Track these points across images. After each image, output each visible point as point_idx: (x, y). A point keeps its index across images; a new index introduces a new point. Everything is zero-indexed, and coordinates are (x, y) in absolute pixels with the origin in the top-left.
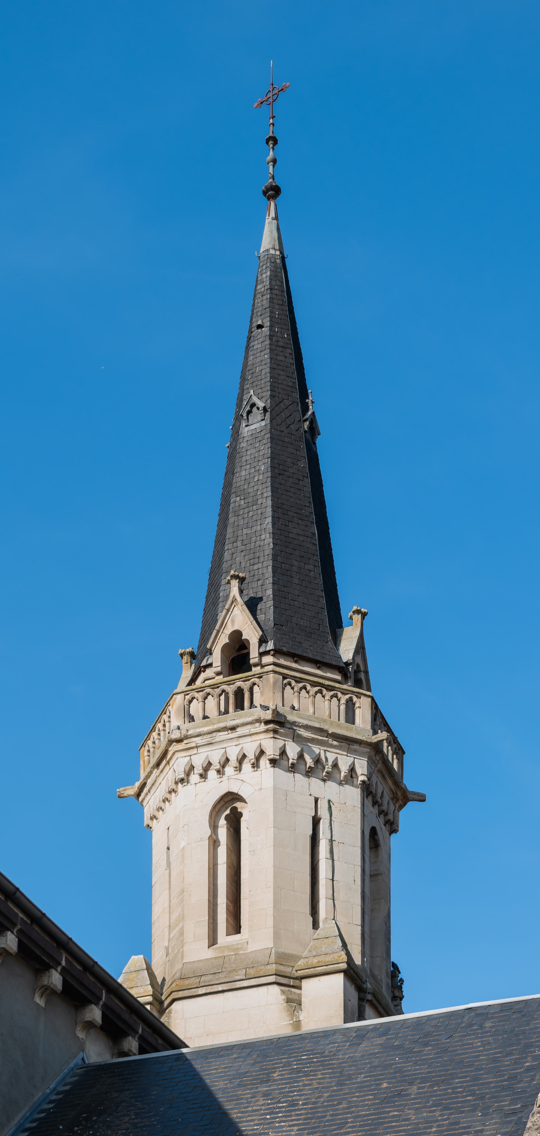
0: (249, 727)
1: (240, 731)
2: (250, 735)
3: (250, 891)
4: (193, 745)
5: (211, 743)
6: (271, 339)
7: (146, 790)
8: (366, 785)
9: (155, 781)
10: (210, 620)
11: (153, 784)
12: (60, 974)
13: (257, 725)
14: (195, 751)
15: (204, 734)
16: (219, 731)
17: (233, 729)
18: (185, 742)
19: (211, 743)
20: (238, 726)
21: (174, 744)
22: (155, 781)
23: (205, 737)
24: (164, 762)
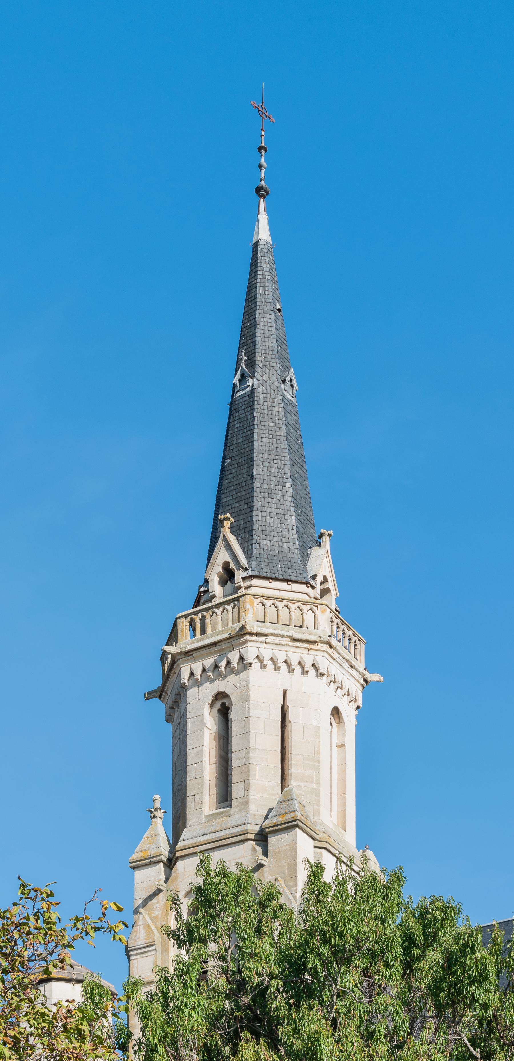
0: (357, 673)
2: (355, 679)
4: (335, 657)
5: (341, 665)
9: (282, 645)
11: (352, 675)
13: (361, 676)
16: (347, 661)
18: (332, 650)
19: (341, 665)
21: (328, 646)
22: (282, 645)
23: (341, 658)
24: (307, 645)
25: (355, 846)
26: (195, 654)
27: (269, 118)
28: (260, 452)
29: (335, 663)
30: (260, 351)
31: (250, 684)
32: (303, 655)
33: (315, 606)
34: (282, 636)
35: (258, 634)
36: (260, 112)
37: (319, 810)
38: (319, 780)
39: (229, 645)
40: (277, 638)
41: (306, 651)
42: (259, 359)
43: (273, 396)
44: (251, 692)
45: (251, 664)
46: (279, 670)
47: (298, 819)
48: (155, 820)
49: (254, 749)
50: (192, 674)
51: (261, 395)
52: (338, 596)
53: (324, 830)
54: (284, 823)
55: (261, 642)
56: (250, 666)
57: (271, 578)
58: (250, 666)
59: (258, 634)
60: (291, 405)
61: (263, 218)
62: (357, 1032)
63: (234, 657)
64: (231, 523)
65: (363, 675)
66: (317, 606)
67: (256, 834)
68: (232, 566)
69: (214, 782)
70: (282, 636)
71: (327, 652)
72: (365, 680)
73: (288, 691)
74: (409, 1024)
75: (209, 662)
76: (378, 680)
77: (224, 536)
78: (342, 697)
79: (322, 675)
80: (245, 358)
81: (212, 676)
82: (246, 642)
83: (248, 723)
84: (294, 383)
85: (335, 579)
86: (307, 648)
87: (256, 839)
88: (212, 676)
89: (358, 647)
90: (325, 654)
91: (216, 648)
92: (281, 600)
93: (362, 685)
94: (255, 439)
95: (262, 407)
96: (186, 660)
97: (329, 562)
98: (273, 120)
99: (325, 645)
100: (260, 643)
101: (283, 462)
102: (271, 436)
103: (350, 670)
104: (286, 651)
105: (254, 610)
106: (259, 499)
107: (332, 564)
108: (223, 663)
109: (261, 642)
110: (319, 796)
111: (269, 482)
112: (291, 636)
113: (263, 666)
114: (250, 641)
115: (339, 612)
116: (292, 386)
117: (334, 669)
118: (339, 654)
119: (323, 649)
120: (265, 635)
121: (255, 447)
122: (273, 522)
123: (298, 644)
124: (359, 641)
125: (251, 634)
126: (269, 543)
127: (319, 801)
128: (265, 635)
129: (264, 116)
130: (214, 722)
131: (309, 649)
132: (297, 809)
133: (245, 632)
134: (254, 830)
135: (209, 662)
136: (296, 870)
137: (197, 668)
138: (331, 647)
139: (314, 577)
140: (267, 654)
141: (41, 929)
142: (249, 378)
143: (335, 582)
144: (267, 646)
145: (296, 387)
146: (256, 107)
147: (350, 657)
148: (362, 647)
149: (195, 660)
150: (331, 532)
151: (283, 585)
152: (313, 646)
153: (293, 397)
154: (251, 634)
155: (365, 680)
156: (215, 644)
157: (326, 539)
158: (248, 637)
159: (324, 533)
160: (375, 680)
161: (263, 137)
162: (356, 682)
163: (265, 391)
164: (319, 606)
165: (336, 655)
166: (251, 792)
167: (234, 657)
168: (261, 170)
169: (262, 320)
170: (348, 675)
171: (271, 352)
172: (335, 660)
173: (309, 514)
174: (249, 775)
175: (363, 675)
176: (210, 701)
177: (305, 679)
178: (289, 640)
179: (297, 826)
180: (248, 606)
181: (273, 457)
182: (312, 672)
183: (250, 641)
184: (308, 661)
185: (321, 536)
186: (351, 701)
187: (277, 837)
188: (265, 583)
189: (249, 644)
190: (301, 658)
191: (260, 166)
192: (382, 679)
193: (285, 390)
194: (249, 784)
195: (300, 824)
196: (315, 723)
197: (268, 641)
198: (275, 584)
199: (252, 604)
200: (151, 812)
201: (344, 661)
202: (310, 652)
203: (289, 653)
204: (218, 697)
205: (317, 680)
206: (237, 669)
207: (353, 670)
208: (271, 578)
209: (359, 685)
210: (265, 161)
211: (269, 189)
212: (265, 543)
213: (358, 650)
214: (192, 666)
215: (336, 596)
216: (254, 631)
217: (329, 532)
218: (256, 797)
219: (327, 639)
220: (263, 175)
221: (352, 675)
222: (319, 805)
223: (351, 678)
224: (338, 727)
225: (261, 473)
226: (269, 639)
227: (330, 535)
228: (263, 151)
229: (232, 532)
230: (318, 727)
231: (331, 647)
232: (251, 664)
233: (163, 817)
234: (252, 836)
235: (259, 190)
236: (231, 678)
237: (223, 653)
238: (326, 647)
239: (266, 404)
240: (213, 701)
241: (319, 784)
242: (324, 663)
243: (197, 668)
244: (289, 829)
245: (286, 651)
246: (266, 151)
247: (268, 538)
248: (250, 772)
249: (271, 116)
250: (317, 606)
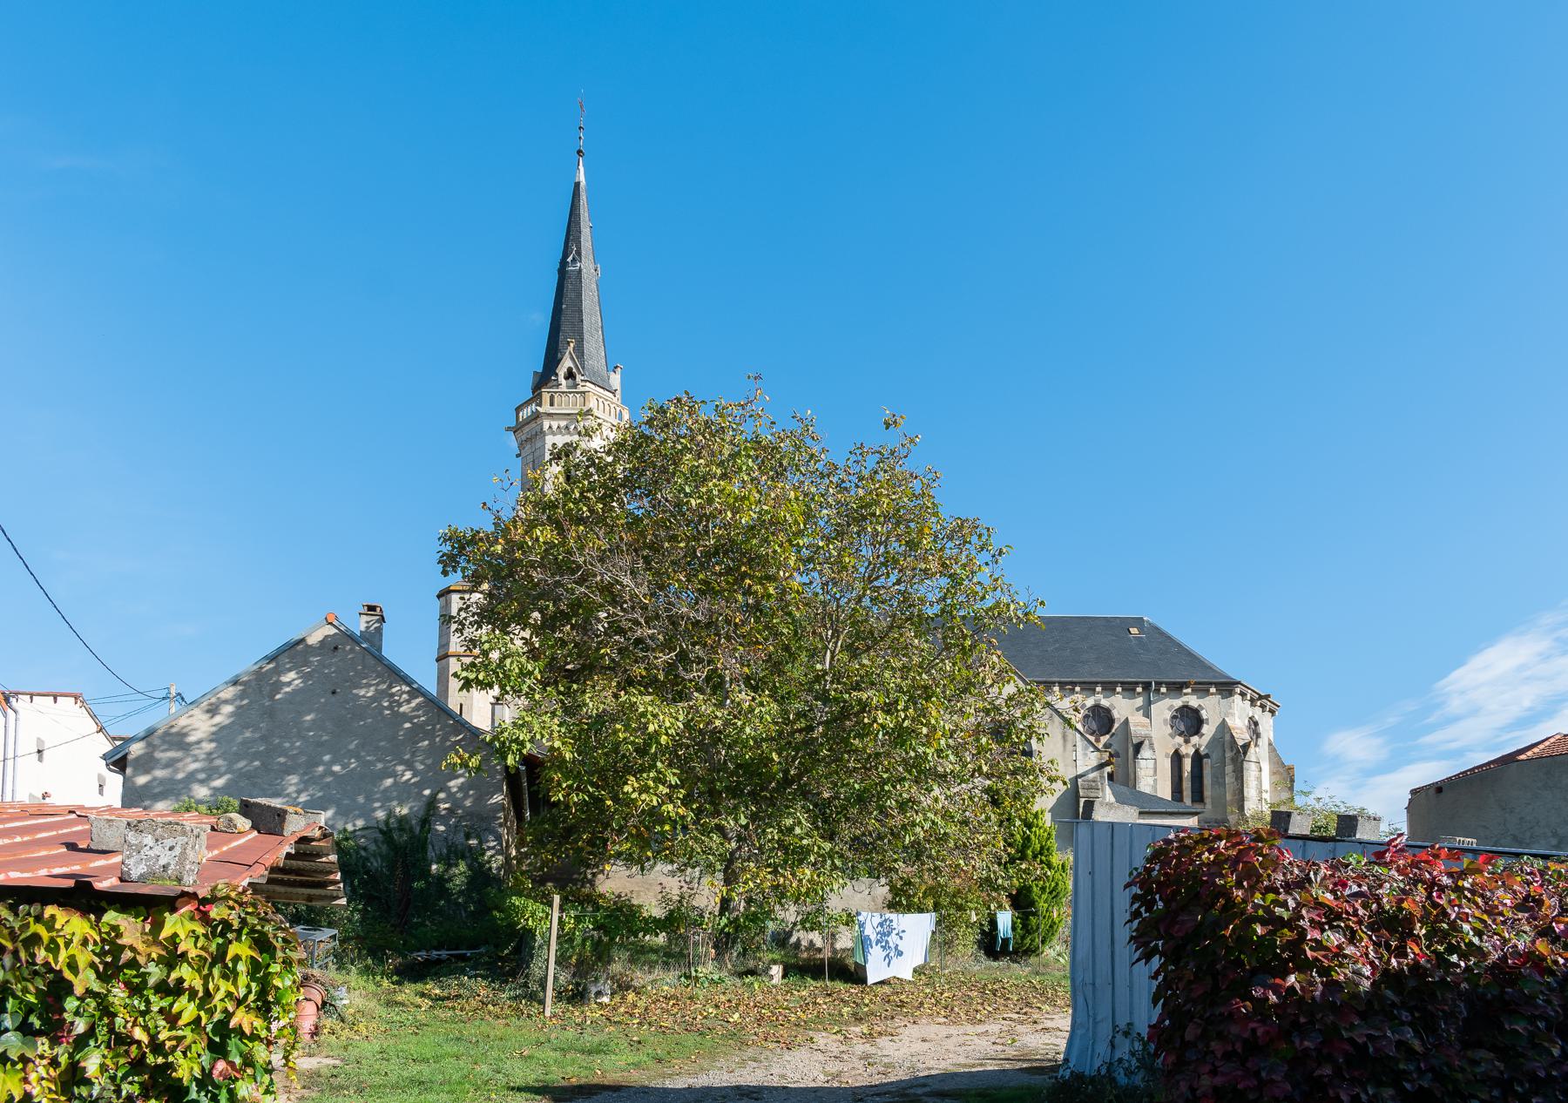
42: (583, 253)
50: (550, 427)
54: (33, 816)
61: (581, 168)
62: (693, 850)
68: (574, 370)
74: (809, 959)
75: (563, 423)
122: (594, 352)
135: (563, 423)
141: (170, 903)
149: (554, 420)
151: (601, 390)
156: (569, 414)
185: (616, 367)
188: (592, 386)
198: (598, 389)
235: (580, 128)
243: (555, 425)
244: (563, 290)
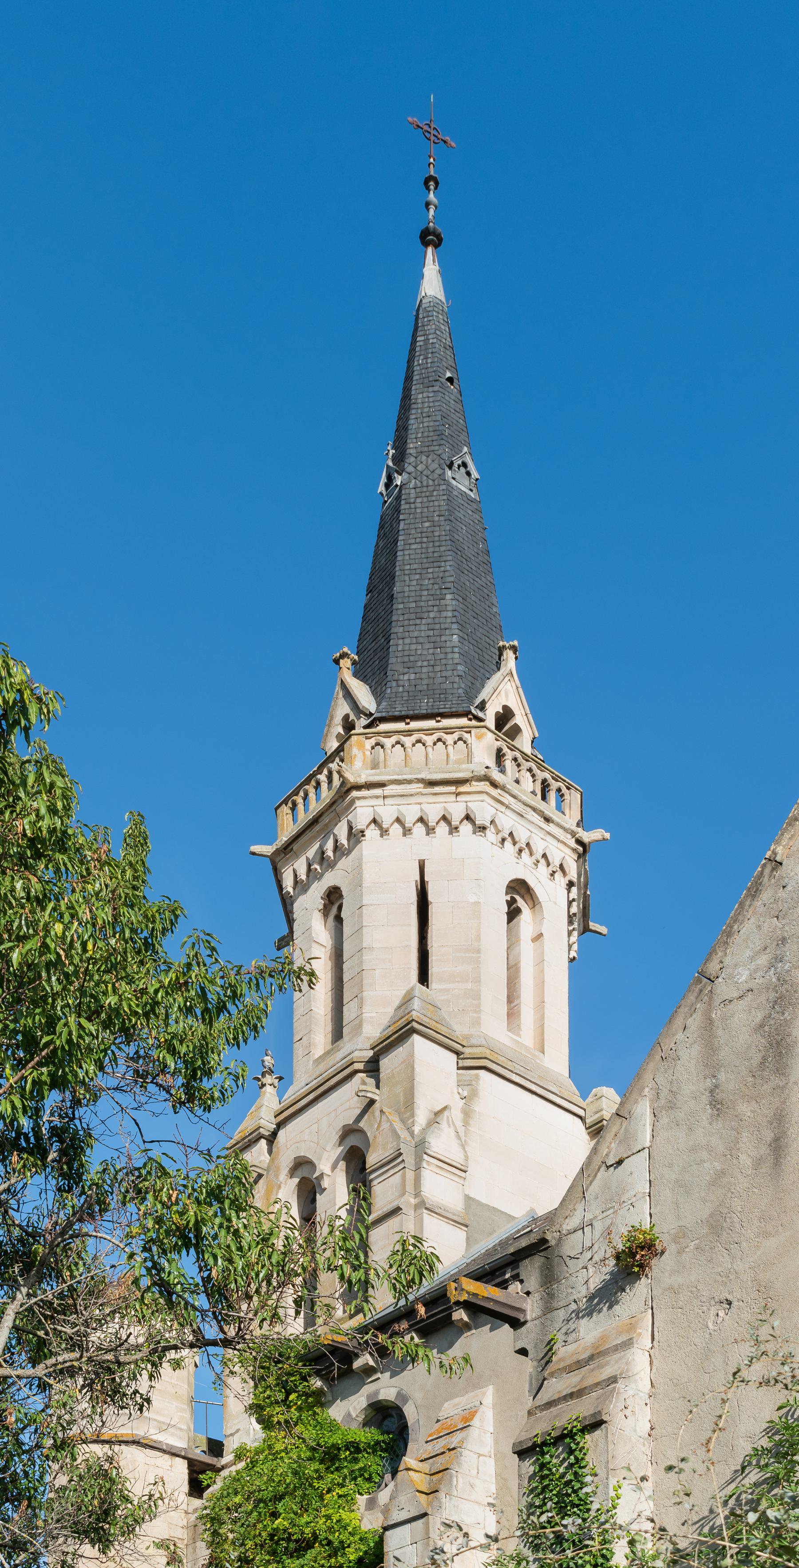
0: (561, 831)
1: (552, 828)
2: (559, 840)
3: (652, 1429)
4: (506, 802)
5: (522, 816)
6: (392, 597)
7: (378, 791)
8: (212, 1098)
9: (412, 795)
10: (369, 669)
11: (549, 833)
12: (518, 1267)
13: (569, 836)
14: (503, 809)
15: (520, 801)
16: (534, 810)
17: (547, 820)
18: (499, 791)
19: (522, 816)
20: (553, 822)
21: (488, 783)
22: (412, 795)
23: (519, 804)
24: (452, 789)
25: (567, 1075)
26: (295, 846)
27: (445, 142)
28: (406, 562)
29: (508, 812)
30: (414, 436)
31: (364, 860)
32: (447, 805)
33: (467, 732)
34: (409, 782)
35: (370, 786)
36: (427, 134)
37: (479, 1018)
38: (480, 977)
39: (332, 815)
40: (402, 786)
41: (452, 798)
43: (431, 489)
44: (365, 872)
45: (362, 832)
46: (411, 834)
47: (413, 1020)
48: (264, 1089)
49: (371, 949)
51: (413, 491)
52: (537, 735)
53: (484, 1043)
55: (377, 797)
56: (363, 836)
57: (407, 717)
58: (363, 836)
59: (370, 786)
60: (465, 499)
63: (341, 830)
64: (354, 663)
65: (573, 834)
66: (470, 732)
67: (367, 1062)
69: (329, 1017)
70: (409, 782)
71: (487, 793)
72: (579, 842)
73: (426, 862)
76: (600, 837)
77: (342, 681)
78: (534, 866)
79: (483, 828)
80: (392, 452)
81: (319, 870)
82: (353, 802)
83: (361, 916)
84: (472, 467)
85: (528, 712)
86: (454, 793)
87: (369, 1068)
88: (319, 870)
89: (567, 797)
90: (485, 797)
91: (317, 828)
92: (409, 733)
93: (574, 850)
94: (400, 548)
95: (413, 506)
96: (287, 860)
97: (515, 688)
98: (453, 144)
99: (483, 783)
100: (375, 800)
101: (442, 569)
102: (425, 540)
103: (543, 824)
104: (420, 804)
105: (364, 754)
106: (399, 624)
107: (520, 690)
108: (330, 845)
109: (377, 797)
110: (480, 999)
111: (418, 599)
112: (423, 779)
113: (384, 832)
114: (359, 798)
115: (543, 761)
116: (468, 474)
117: (507, 821)
118: (514, 797)
119: (479, 789)
120: (381, 785)
121: (399, 558)
123: (437, 789)
124: (568, 788)
125: (358, 787)
126: (413, 676)
127: (479, 1005)
128: (381, 785)
129: (433, 138)
130: (329, 936)
131: (458, 794)
132: (604, 1106)
133: (349, 786)
134: (364, 1057)
136: (413, 1093)
137: (301, 866)
138: (494, 785)
139: (482, 706)
140: (387, 814)
142: (396, 475)
143: (530, 716)
144: (387, 801)
145: (475, 474)
146: (418, 126)
147: (542, 805)
148: (573, 799)
150: (516, 643)
152: (462, 789)
153: (471, 490)
154: (358, 787)
155: (579, 842)
157: (509, 655)
158: (355, 794)
159: (504, 647)
160: (596, 838)
161: (432, 166)
162: (561, 846)
163: (419, 484)
164: (473, 731)
165: (508, 799)
166: (366, 1009)
167: (341, 830)
168: (428, 210)
169: (420, 396)
170: (541, 834)
171: (432, 434)
172: (507, 807)
173: (492, 637)
174: (362, 985)
175: (573, 834)
176: (321, 907)
177: (455, 839)
178: (421, 785)
179: (414, 1031)
180: (355, 751)
181: (427, 565)
182: (467, 828)
183: (359, 798)
184: (457, 812)
186: (554, 872)
187: (390, 1056)
189: (358, 803)
190: (445, 809)
191: (427, 204)
192: (607, 835)
193: (454, 479)
194: (362, 998)
195: (415, 1024)
196: (472, 898)
197: (387, 793)
199: (361, 746)
200: (258, 1079)
201: (529, 809)
202: (459, 798)
203: (424, 806)
204: (332, 898)
205: (478, 839)
206: (346, 846)
207: (551, 825)
208: (407, 717)
209: (569, 851)
210: (435, 196)
211: (439, 229)
212: (406, 677)
213: (567, 802)
214: (295, 866)
215: (532, 736)
216: (362, 780)
217: (511, 643)
218: (374, 1015)
219: (483, 772)
220: (431, 217)
221: (549, 833)
222: (479, 1012)
223: (549, 838)
224: (534, 913)
225: (407, 589)
226: (389, 790)
227: (514, 649)
228: (432, 183)
229: (356, 675)
230: (477, 904)
231: (494, 785)
232: (362, 832)
233: (276, 1085)
234: (360, 1066)
236: (343, 863)
237: (328, 831)
238: (484, 786)
239: (419, 500)
240: (325, 905)
241: (480, 981)
242: (484, 811)
243: (301, 866)
245: (420, 804)
246: (437, 184)
247: (411, 670)
248: (365, 982)
249: (448, 138)
250: (470, 732)
